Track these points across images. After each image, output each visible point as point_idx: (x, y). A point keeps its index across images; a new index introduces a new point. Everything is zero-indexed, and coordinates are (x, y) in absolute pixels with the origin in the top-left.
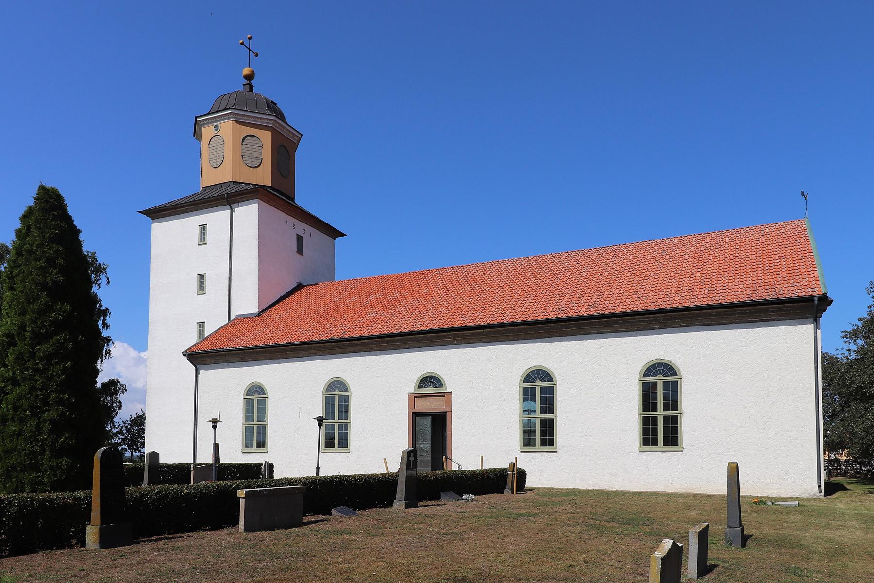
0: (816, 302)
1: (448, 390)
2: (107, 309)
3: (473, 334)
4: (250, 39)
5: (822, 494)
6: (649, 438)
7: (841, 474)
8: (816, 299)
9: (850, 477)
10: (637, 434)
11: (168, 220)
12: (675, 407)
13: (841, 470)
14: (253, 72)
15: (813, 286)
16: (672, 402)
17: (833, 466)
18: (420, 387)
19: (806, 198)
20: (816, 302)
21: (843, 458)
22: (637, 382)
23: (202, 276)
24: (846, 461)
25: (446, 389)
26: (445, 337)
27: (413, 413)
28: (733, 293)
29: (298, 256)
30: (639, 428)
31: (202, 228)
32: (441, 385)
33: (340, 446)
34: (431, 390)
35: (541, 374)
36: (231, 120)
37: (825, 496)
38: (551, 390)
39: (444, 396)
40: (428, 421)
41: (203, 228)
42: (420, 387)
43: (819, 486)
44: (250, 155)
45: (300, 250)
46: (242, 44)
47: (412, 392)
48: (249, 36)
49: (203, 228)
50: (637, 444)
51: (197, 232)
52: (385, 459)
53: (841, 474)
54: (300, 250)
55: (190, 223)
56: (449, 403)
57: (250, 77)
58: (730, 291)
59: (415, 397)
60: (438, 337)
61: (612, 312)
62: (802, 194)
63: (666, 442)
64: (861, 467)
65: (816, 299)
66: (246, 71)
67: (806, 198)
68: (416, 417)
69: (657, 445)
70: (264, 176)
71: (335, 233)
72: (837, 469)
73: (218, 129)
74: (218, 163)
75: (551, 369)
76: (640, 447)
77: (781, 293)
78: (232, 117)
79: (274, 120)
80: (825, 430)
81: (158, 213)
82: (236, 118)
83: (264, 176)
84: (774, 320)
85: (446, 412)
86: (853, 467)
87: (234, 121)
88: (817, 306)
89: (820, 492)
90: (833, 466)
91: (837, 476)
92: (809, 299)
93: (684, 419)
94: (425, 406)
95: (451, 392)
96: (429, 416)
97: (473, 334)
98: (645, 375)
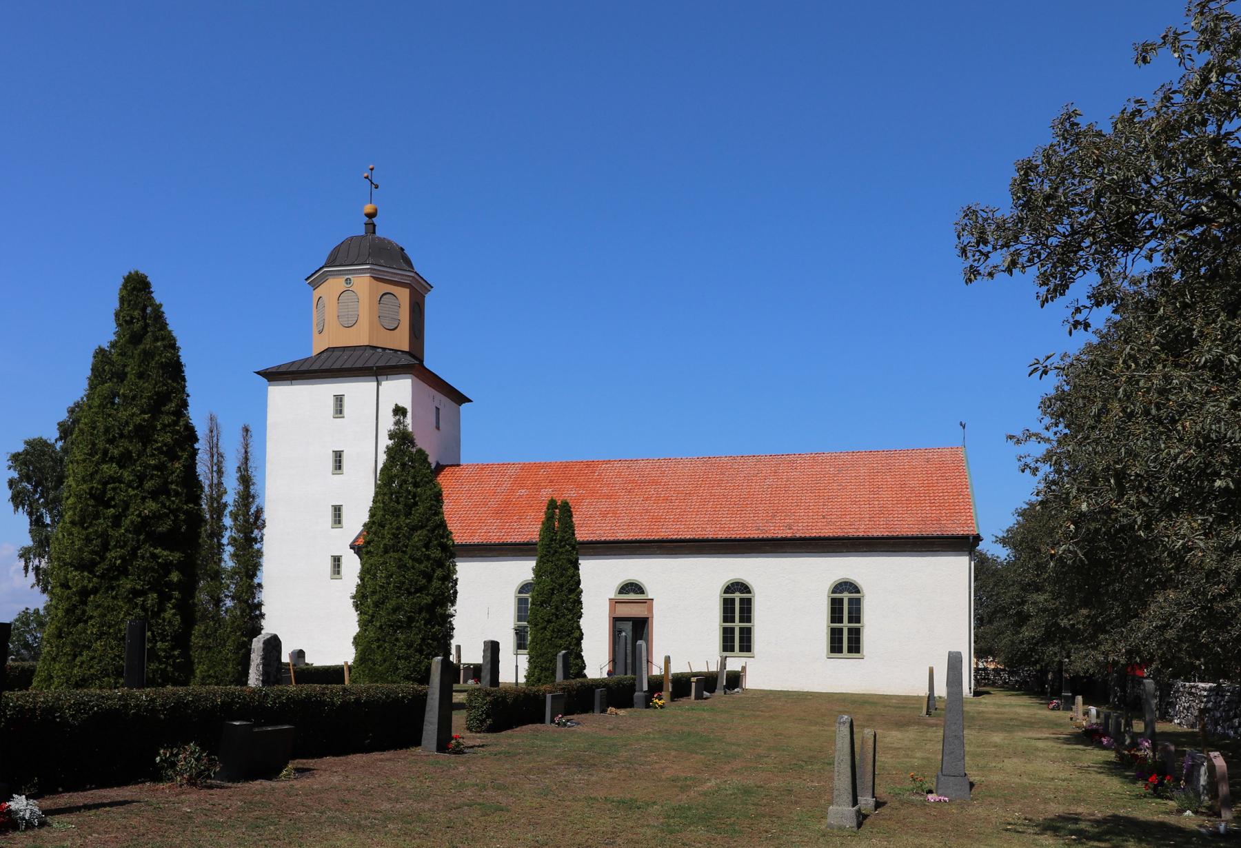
0: (971, 541)
1: (650, 597)
2: (26, 442)
3: (676, 547)
4: (372, 169)
5: (972, 694)
6: (835, 646)
7: (989, 685)
8: (971, 538)
9: (997, 687)
10: (826, 643)
11: (292, 384)
12: (858, 620)
13: (989, 679)
14: (376, 210)
15: (969, 525)
16: (856, 616)
17: (981, 675)
18: (620, 592)
19: (964, 428)
20: (971, 541)
21: (992, 666)
22: (826, 597)
23: (338, 456)
24: (993, 670)
25: (647, 596)
26: (648, 547)
27: (614, 618)
28: (907, 526)
29: (437, 431)
30: (827, 638)
31: (337, 398)
32: (643, 592)
33: (741, 650)
34: (632, 596)
35: (847, 586)
36: (368, 275)
37: (974, 696)
38: (749, 601)
39: (646, 602)
40: (628, 627)
41: (339, 400)
42: (620, 592)
43: (970, 688)
44: (387, 315)
45: (438, 428)
46: (367, 178)
47: (613, 597)
48: (371, 167)
49: (339, 400)
50: (825, 651)
51: (331, 403)
52: (707, 662)
53: (989, 685)
54: (438, 428)
55: (322, 392)
56: (651, 609)
57: (371, 216)
58: (904, 523)
59: (616, 602)
60: (643, 547)
61: (807, 535)
62: (961, 424)
63: (850, 651)
64: (1009, 677)
65: (971, 538)
66: (369, 208)
67: (964, 428)
68: (616, 621)
69: (842, 653)
70: (401, 340)
71: (460, 399)
72: (984, 679)
73: (350, 283)
74: (350, 322)
75: (646, 586)
76: (720, 653)
77: (944, 529)
78: (369, 273)
79: (413, 277)
80: (975, 676)
81: (276, 375)
82: (373, 273)
83: (401, 340)
84: (939, 551)
85: (648, 618)
86: (1001, 678)
87: (371, 277)
88: (972, 543)
89: (971, 693)
90: (981, 675)
91: (984, 686)
92: (966, 537)
93: (865, 631)
94: (625, 611)
95: (653, 600)
96: (630, 621)
97: (676, 547)
98: (833, 592)
